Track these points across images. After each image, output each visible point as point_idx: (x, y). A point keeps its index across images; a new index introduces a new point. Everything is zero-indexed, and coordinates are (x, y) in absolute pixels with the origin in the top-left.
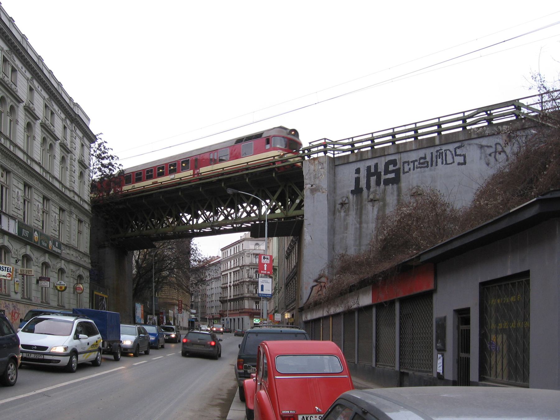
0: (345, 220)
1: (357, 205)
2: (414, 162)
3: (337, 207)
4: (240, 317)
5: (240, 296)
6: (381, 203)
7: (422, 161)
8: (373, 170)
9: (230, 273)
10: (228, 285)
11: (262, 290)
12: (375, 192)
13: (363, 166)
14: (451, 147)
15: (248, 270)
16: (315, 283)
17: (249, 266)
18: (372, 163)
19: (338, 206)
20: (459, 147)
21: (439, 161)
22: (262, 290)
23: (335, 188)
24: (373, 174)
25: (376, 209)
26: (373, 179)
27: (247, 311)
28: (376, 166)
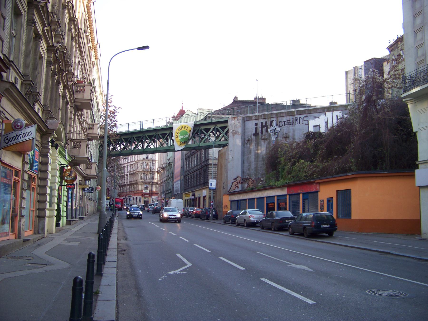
1: (256, 141)
2: (284, 122)
3: (246, 142)
4: (135, 197)
5: (135, 182)
7: (288, 122)
8: (264, 125)
9: (128, 166)
10: (126, 174)
11: (211, 186)
12: (265, 135)
14: (302, 116)
16: (234, 181)
17: (142, 160)
18: (263, 121)
19: (246, 141)
20: (306, 117)
21: (297, 122)
22: (211, 186)
24: (264, 127)
25: (266, 144)
26: (264, 129)
27: (139, 192)
28: (266, 123)
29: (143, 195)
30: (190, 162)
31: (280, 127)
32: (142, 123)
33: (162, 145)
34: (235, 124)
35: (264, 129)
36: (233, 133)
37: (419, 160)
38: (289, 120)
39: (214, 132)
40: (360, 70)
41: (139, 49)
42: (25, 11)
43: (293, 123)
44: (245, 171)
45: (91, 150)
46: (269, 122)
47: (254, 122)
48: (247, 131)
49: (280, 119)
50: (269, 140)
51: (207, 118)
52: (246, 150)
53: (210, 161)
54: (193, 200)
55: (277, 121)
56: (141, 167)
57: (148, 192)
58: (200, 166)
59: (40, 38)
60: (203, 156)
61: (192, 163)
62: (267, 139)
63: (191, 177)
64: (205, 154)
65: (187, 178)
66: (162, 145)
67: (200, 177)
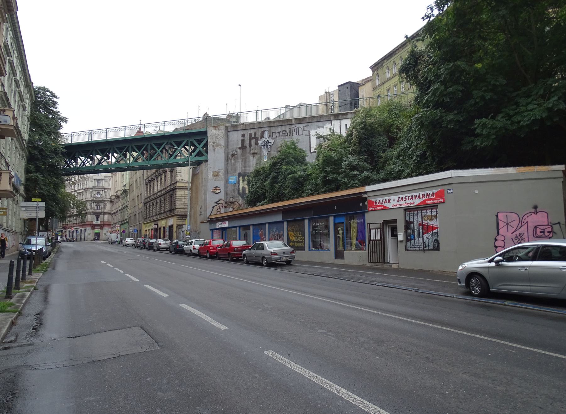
0: (234, 164)
2: (279, 132)
3: (230, 157)
4: (83, 229)
6: (259, 156)
8: (253, 136)
15: (91, 192)
17: (92, 188)
19: (230, 157)
20: (306, 126)
21: (295, 133)
23: (228, 145)
24: (253, 138)
26: (253, 141)
28: (255, 134)
29: (93, 226)
30: (152, 187)
31: (273, 139)
32: (90, 133)
34: (215, 135)
35: (253, 141)
36: (213, 146)
39: (186, 147)
40: (332, 96)
43: (291, 134)
44: (229, 192)
45: (7, 158)
46: (260, 133)
47: (240, 133)
48: (230, 143)
49: (273, 130)
50: (261, 154)
53: (178, 185)
54: (156, 230)
56: (91, 195)
57: (99, 223)
58: (165, 190)
60: (169, 179)
61: (153, 188)
63: (153, 205)
64: (172, 176)
65: (148, 206)
66: (118, 162)
67: (165, 204)
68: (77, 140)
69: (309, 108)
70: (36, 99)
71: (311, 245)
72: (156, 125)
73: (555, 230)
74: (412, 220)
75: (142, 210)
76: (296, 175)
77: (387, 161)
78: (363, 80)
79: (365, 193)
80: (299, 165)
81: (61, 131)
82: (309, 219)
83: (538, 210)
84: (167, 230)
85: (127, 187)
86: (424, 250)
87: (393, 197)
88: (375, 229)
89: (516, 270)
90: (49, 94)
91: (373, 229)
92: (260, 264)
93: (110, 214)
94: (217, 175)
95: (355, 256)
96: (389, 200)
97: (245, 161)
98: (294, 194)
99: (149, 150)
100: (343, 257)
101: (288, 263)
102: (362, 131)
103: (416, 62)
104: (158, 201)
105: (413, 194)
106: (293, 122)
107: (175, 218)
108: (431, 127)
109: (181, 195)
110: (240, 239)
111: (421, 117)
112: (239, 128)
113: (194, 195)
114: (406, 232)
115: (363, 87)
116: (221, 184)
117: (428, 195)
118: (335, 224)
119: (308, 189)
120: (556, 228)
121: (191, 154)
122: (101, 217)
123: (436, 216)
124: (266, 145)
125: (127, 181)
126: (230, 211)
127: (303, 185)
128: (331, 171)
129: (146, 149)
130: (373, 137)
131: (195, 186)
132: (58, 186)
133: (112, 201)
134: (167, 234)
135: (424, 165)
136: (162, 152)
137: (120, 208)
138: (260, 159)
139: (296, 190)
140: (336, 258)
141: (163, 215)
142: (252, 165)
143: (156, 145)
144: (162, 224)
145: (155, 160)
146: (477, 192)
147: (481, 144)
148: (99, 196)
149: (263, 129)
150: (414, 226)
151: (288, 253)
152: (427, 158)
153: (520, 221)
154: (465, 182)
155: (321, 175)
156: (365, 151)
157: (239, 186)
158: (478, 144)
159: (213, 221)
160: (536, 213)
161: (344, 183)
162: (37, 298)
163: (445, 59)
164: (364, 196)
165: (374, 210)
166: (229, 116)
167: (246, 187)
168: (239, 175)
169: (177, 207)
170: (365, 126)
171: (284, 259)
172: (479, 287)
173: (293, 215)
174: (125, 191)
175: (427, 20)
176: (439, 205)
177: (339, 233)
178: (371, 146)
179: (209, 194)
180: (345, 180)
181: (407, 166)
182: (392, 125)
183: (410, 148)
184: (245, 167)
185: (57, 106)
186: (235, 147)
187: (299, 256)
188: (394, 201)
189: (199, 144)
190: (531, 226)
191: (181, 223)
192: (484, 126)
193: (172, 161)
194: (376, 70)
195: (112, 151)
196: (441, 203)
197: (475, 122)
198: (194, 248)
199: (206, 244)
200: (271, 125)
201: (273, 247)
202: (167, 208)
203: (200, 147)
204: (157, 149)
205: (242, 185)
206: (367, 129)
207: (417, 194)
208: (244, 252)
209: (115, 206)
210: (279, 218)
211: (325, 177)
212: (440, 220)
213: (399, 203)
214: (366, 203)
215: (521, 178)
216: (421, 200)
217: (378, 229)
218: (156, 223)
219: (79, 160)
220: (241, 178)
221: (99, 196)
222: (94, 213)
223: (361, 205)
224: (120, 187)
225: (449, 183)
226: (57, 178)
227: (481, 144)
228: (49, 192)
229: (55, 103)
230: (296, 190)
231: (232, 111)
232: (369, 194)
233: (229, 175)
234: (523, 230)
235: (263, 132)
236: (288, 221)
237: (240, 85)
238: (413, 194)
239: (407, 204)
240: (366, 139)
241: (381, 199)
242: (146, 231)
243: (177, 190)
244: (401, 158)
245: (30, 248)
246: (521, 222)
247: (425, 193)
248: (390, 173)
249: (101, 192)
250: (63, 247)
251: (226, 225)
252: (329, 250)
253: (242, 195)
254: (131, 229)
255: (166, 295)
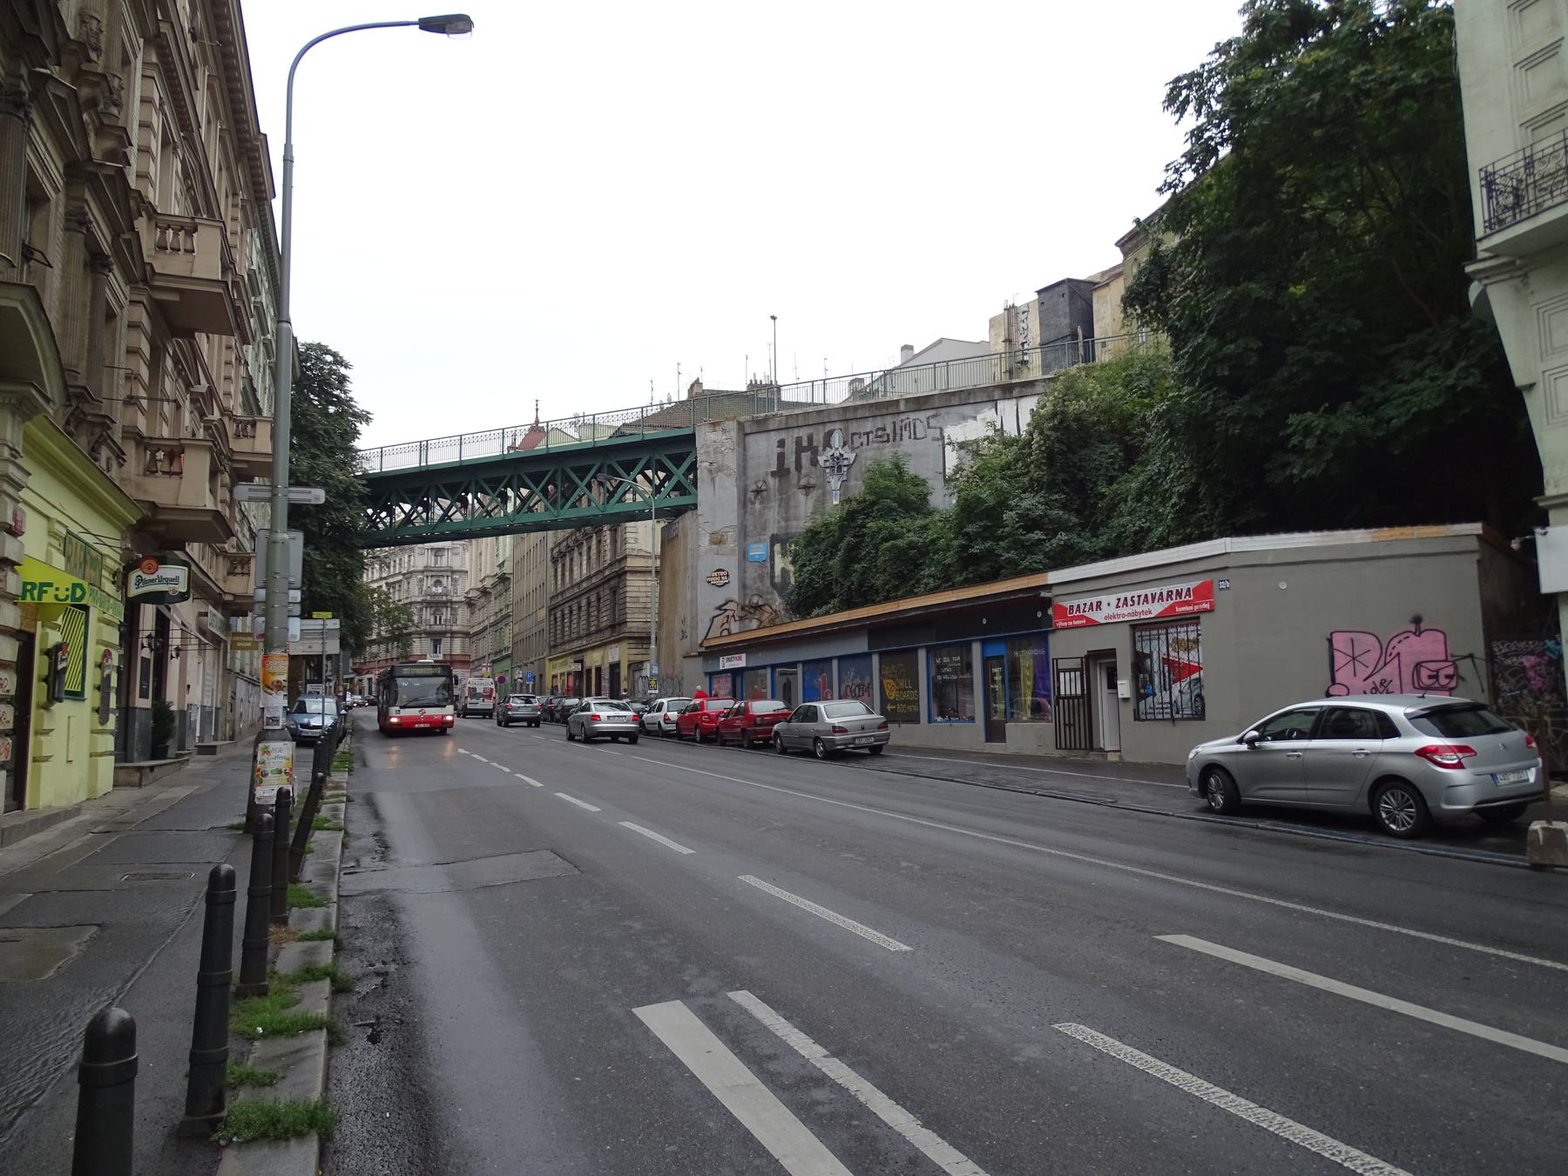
0: (761, 515)
3: (751, 496)
8: (805, 444)
12: (807, 475)
13: (790, 438)
14: (922, 415)
15: (421, 581)
18: (803, 433)
19: (751, 495)
21: (906, 434)
23: (745, 468)
25: (811, 503)
26: (806, 457)
28: (810, 438)
31: (853, 449)
32: (424, 447)
33: (489, 513)
34: (714, 444)
35: (806, 457)
37: (1550, 491)
38: (884, 429)
40: (1023, 317)
41: (429, 25)
42: (57, 190)
43: (896, 436)
45: (252, 519)
47: (775, 437)
48: (751, 463)
49: (854, 427)
50: (824, 487)
51: (619, 433)
52: (750, 520)
53: (631, 563)
54: (578, 675)
55: (844, 431)
56: (421, 589)
58: (600, 577)
59: (108, 267)
60: (608, 548)
62: (813, 487)
64: (614, 541)
66: (489, 513)
67: (599, 610)
68: (394, 464)
69: (941, 371)
70: (303, 373)
71: (935, 710)
72: (576, 421)
73: (1462, 672)
74: (1147, 651)
75: (544, 625)
76: (900, 542)
77: (1116, 505)
78: (1103, 274)
79: (1048, 587)
80: (911, 517)
81: (357, 444)
82: (929, 649)
83: (1423, 626)
84: (606, 674)
85: (508, 569)
86: (1173, 719)
87: (1106, 597)
88: (1070, 670)
89: (1283, 756)
90: (329, 358)
91: (1064, 671)
92: (810, 754)
93: (467, 635)
94: (720, 542)
95: (1027, 735)
96: (1099, 604)
97: (786, 504)
98: (896, 588)
99: (559, 483)
100: (1002, 738)
101: (876, 751)
102: (1054, 435)
103: (1163, 277)
104: (584, 603)
105: (1149, 591)
106: (902, 407)
107: (624, 645)
108: (1194, 431)
109: (639, 589)
110: (773, 698)
111: (1169, 410)
112: (772, 425)
113: (667, 589)
114: (1135, 678)
115: (1104, 291)
116: (731, 563)
117: (1179, 593)
118: (986, 661)
119: (930, 576)
120: (1465, 667)
121: (657, 490)
122: (445, 642)
123: (1196, 642)
124: (837, 465)
125: (508, 553)
126: (754, 629)
127: (917, 566)
128: (977, 534)
129: (552, 481)
130: (1086, 445)
131: (666, 568)
132: (351, 573)
133: (470, 603)
134: (605, 684)
135: (1194, 519)
136: (589, 486)
137: (492, 620)
138: (822, 501)
139: (902, 578)
140: (988, 740)
141: (594, 638)
142: (804, 513)
143: (574, 470)
144: (594, 659)
145: (574, 506)
146: (1283, 586)
147: (1303, 471)
148: (440, 590)
149: (829, 427)
150: (1154, 665)
151: (871, 728)
152: (1199, 502)
153: (1383, 651)
154: (1256, 565)
155: (955, 543)
156: (1065, 482)
157: (772, 566)
158: (1295, 471)
159: (712, 653)
160: (1418, 633)
161: (1009, 561)
162: (359, 814)
163: (1217, 279)
164: (1044, 594)
165: (1068, 628)
166: (754, 386)
167: (791, 568)
168: (774, 539)
169: (629, 617)
170: (1061, 422)
171: (863, 741)
172: (1227, 795)
173: (893, 637)
174: (503, 579)
175: (1168, 195)
176: (1203, 617)
177: (994, 682)
178: (1080, 469)
179: (703, 590)
180: (1012, 555)
181: (1159, 518)
182: (1132, 415)
183: (1167, 474)
184: (787, 520)
185: (349, 386)
186: (763, 470)
187: (900, 734)
188: (1109, 608)
189: (678, 466)
190: (1408, 662)
191: (640, 658)
192: (1307, 431)
193: (614, 508)
194: (1131, 250)
195: (473, 487)
196: (1206, 611)
197: (1289, 421)
198: (666, 720)
199: (695, 708)
200: (850, 415)
201: (841, 714)
202: (605, 620)
203: (679, 473)
204: (577, 481)
205: (779, 563)
206: (1068, 428)
207: (1157, 590)
208: (776, 727)
209: (480, 615)
210: (860, 645)
211: (964, 548)
212: (1212, 651)
213: (1120, 611)
214: (1050, 612)
215: (1383, 554)
216: (1166, 604)
217: (1075, 670)
218: (579, 657)
219: (398, 510)
220: (777, 547)
221: (440, 590)
222: (429, 634)
223: (1039, 615)
224: (490, 569)
225: (1222, 566)
226: (352, 557)
227: (1303, 471)
228: (334, 591)
229: (343, 379)
230: (902, 578)
231: (761, 378)
232: (1056, 591)
233: (750, 540)
234: (1390, 671)
235: (830, 433)
236: (881, 654)
237: (774, 318)
238: (1149, 591)
239: (1136, 613)
240: (1063, 453)
241: (1081, 602)
242: (555, 677)
243: (629, 577)
244: (1146, 498)
245: (306, 721)
246: (1386, 655)
247: (1174, 588)
248: (1119, 535)
249: (444, 581)
250: (360, 718)
251: (740, 662)
252: (972, 719)
253: (781, 588)
254: (518, 674)
255: (594, 809)
